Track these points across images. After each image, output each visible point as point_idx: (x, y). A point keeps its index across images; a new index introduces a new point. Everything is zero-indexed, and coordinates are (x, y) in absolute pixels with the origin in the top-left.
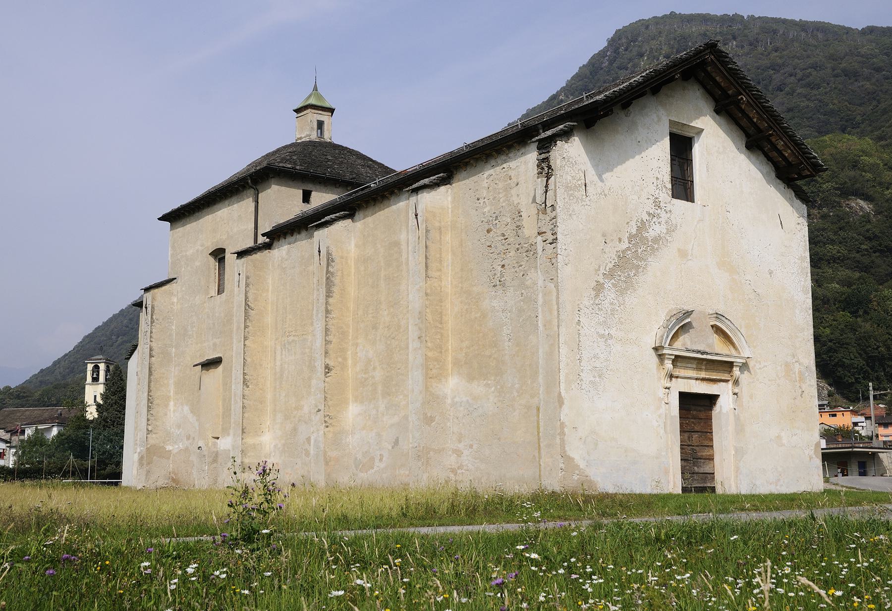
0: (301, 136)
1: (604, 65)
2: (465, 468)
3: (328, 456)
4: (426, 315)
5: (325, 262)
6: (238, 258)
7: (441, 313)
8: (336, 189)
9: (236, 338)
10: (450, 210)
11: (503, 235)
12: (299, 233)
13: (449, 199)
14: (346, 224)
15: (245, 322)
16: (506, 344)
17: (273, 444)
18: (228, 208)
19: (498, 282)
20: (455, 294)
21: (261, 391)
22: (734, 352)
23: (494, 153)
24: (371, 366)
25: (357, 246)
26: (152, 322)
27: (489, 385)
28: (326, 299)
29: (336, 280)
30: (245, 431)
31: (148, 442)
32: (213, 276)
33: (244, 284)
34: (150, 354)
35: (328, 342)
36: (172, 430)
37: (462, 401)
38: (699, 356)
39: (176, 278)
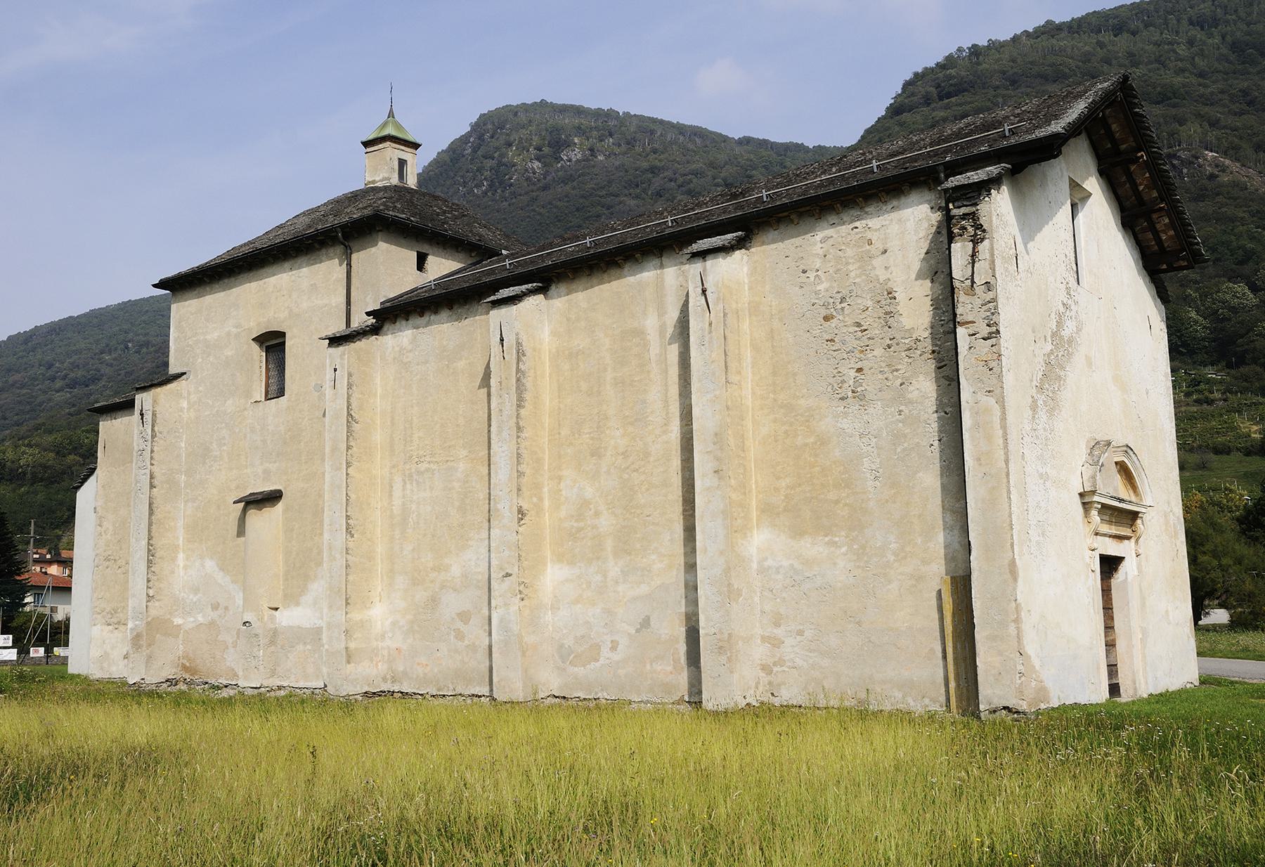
0: (373, 179)
1: (467, 152)
2: (788, 664)
3: (525, 643)
4: (728, 439)
5: (515, 356)
6: (330, 345)
7: (743, 435)
8: (456, 254)
9: (330, 463)
10: (746, 286)
11: (859, 325)
12: (436, 312)
13: (745, 269)
14: (538, 302)
15: (347, 440)
16: (870, 483)
17: (390, 620)
18: (290, 273)
19: (850, 393)
20: (762, 409)
21: (369, 542)
22: (1133, 499)
23: (838, 205)
24: (590, 510)
25: (554, 333)
26: (153, 437)
27: (836, 543)
28: (518, 410)
29: (528, 382)
30: (349, 601)
31: (149, 613)
32: (258, 371)
33: (346, 384)
34: (151, 483)
35: (520, 474)
36: (182, 594)
37: (781, 566)
38: (1116, 504)
39: (185, 373)
